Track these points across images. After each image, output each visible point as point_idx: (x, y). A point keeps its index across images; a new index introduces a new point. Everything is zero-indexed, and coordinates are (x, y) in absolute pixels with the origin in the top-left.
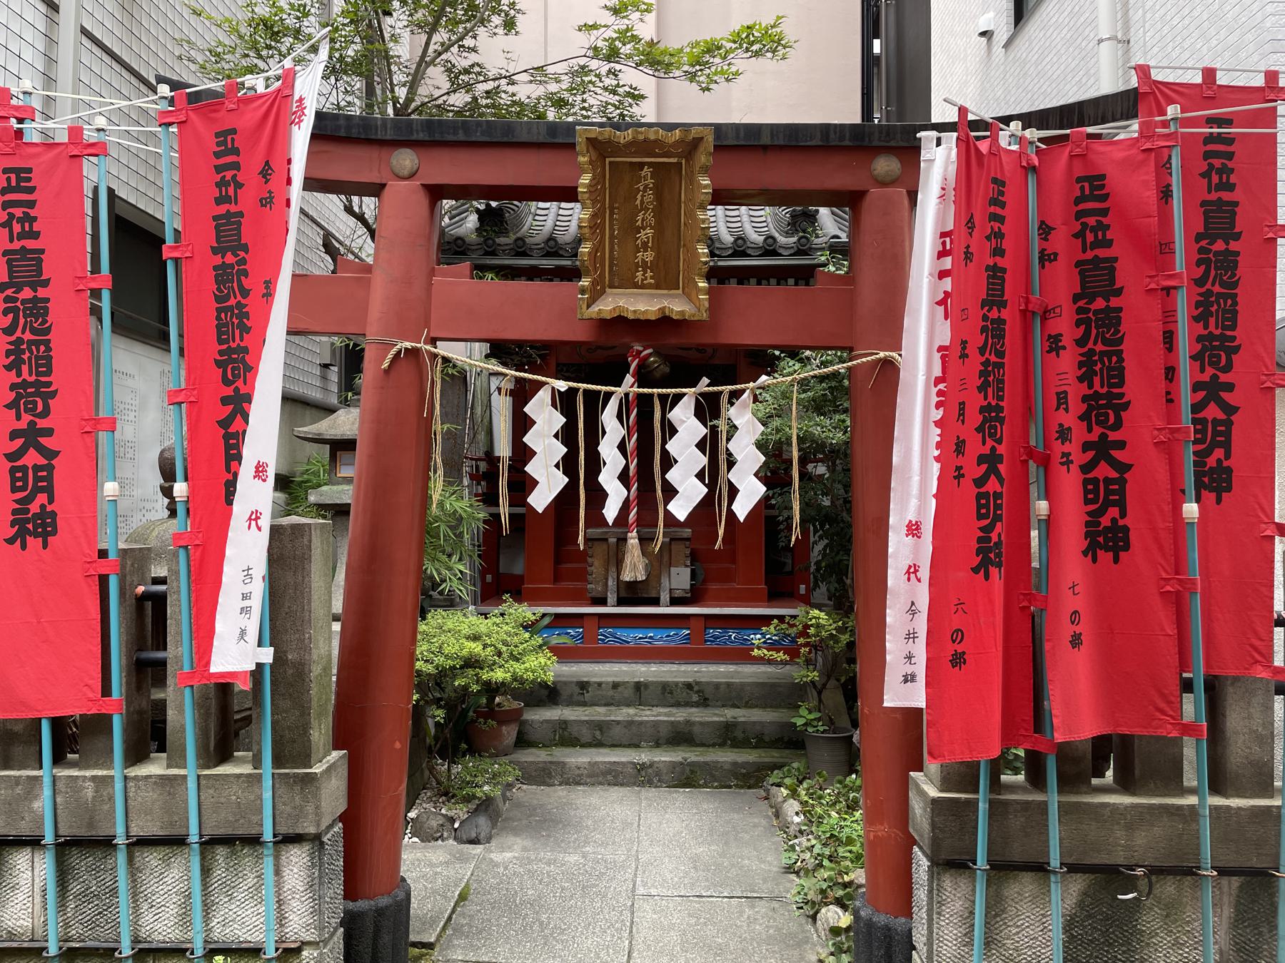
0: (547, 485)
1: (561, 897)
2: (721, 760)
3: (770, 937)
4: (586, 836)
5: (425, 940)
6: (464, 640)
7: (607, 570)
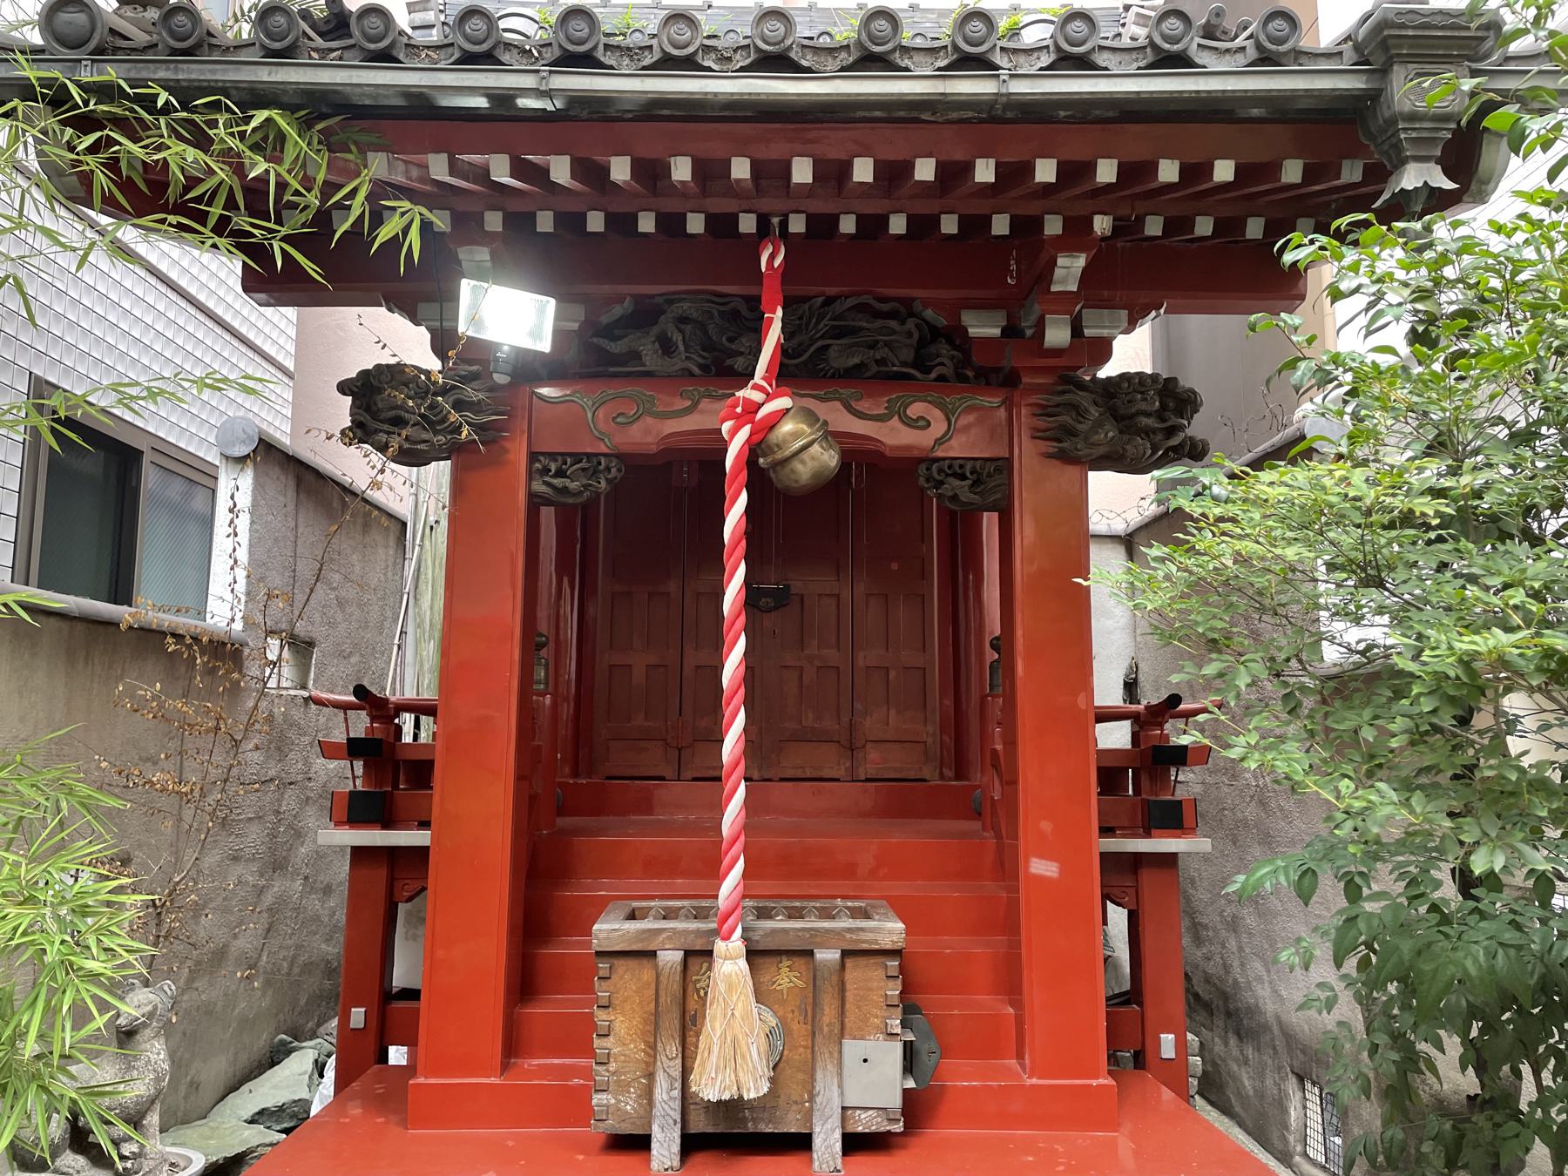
7: (652, 1049)
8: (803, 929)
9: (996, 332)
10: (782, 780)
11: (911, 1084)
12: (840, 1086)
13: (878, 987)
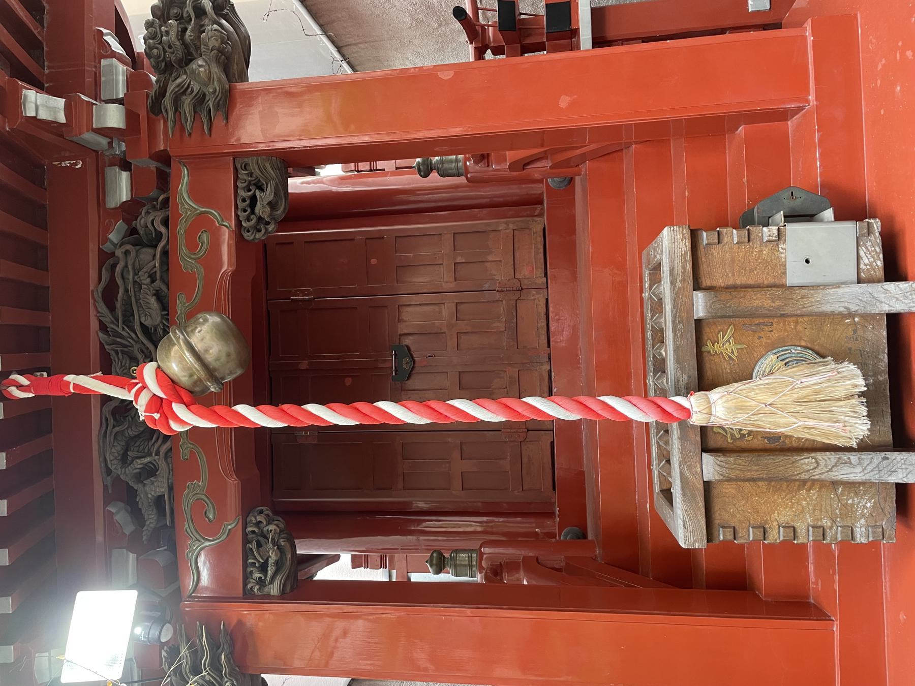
8: (674, 331)
9: (125, 176)
10: (549, 346)
11: (829, 214)
12: (837, 285)
13: (729, 250)
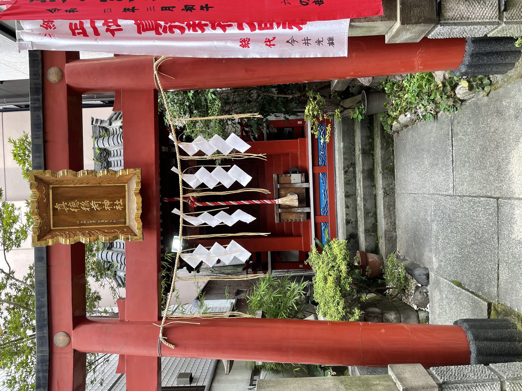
0: (237, 253)
1: (456, 233)
2: (380, 155)
3: (474, 123)
4: (422, 220)
5: (487, 307)
6: (328, 285)
7: (294, 213)
